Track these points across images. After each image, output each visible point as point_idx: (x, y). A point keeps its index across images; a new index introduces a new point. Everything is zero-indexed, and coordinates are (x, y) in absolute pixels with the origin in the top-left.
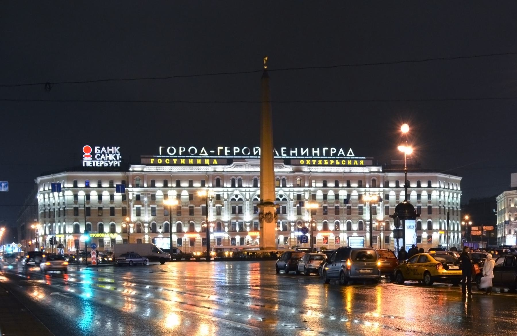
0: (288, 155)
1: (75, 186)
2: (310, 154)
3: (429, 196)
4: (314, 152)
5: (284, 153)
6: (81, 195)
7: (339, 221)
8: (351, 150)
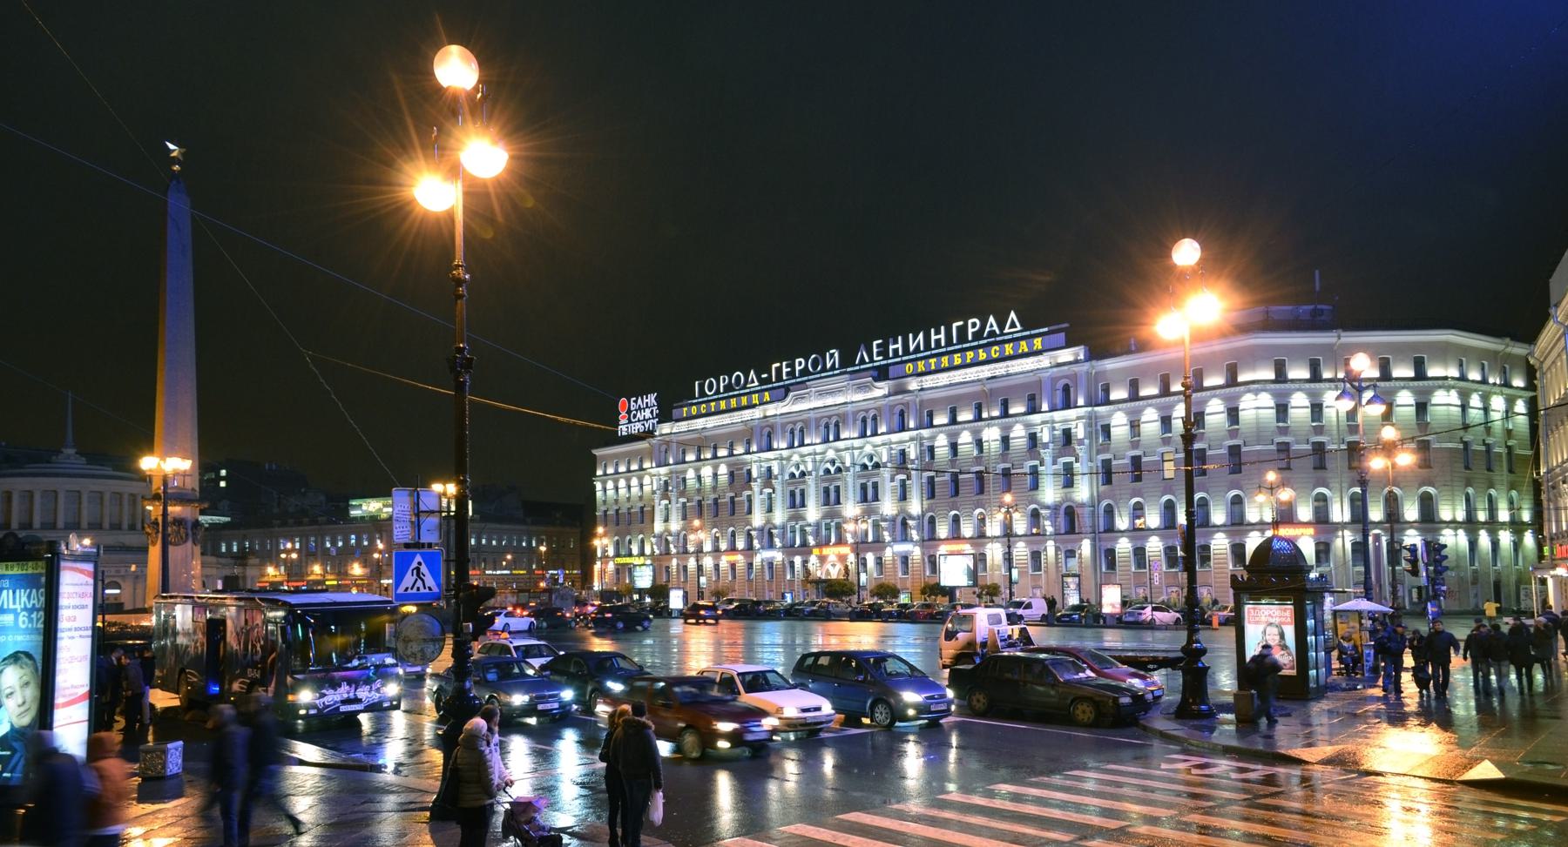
0: (886, 357)
1: (1281, 377)
2: (906, 351)
3: (1233, 414)
4: (933, 337)
5: (879, 354)
6: (1299, 403)
7: (1431, 490)
8: (1013, 315)
